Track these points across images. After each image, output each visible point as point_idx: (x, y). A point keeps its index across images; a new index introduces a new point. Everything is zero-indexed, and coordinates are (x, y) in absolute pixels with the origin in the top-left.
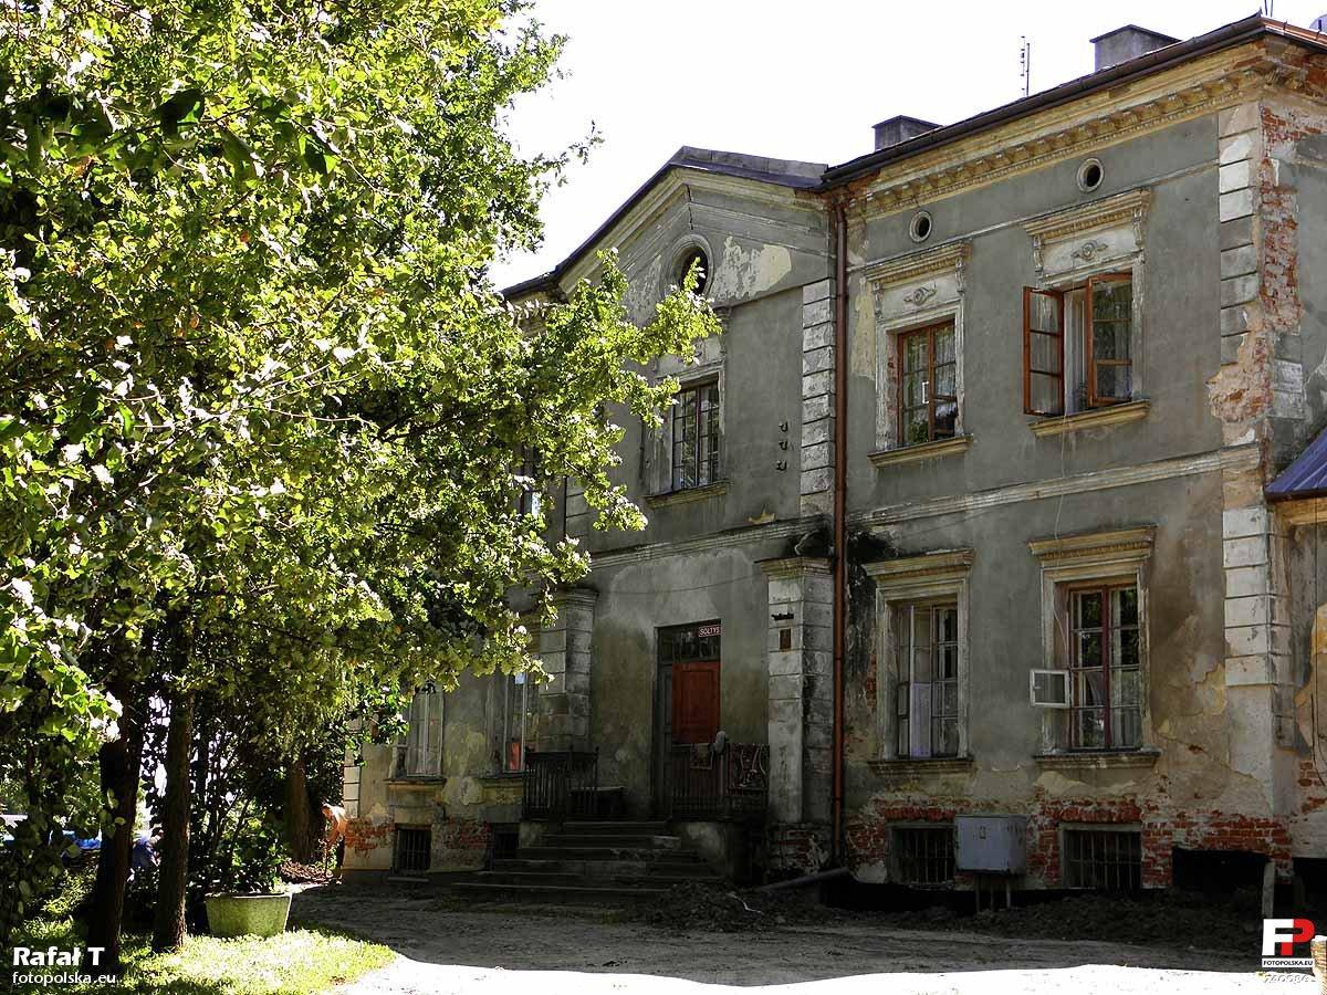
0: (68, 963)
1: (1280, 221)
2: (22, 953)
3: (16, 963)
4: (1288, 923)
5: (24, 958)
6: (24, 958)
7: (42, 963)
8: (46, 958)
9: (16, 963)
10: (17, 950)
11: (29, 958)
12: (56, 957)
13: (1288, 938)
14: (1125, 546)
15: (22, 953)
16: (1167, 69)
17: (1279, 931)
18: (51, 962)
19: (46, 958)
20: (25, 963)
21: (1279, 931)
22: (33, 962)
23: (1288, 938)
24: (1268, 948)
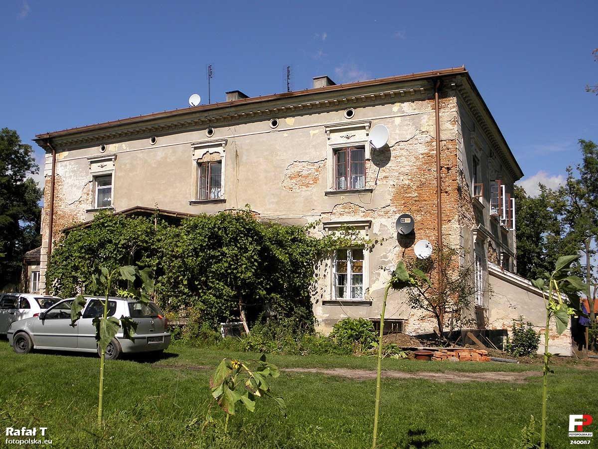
0: (31, 435)
2: (10, 430)
3: (7, 434)
4: (581, 417)
7: (19, 435)
9: (7, 434)
10: (8, 429)
12: (25, 432)
15: (10, 430)
17: (577, 420)
18: (23, 434)
20: (11, 434)
21: (577, 420)
22: (15, 434)
23: (581, 423)
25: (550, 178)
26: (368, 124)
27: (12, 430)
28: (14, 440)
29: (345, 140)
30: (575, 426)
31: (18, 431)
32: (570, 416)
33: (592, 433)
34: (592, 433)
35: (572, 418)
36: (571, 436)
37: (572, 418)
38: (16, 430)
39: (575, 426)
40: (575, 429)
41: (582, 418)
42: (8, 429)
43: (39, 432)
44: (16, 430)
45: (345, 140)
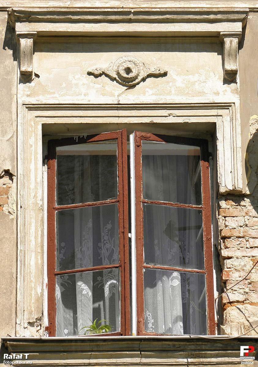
0: (19, 358)
1: (33, 200)
2: (6, 355)
3: (4, 358)
4: (247, 347)
5: (7, 357)
6: (7, 357)
7: (12, 358)
8: (13, 357)
9: (4, 358)
10: (5, 355)
11: (8, 357)
12: (15, 357)
13: (247, 351)
14: (97, 238)
15: (6, 355)
16: (102, 363)
17: (245, 349)
18: (14, 358)
19: (13, 357)
20: (7, 358)
21: (245, 349)
22: (9, 358)
23: (247, 351)
24: (242, 354)
25: (211, 153)
26: (237, 27)
27: (7, 355)
28: (8, 362)
29: (115, 93)
30: (244, 353)
31: (11, 356)
32: (241, 346)
33: (254, 357)
34: (254, 357)
35: (242, 348)
36: (253, 357)
37: (242, 348)
38: (9, 356)
39: (244, 353)
40: (244, 355)
41: (248, 348)
42: (5, 355)
43: (24, 356)
44: (9, 356)
45: (115, 93)
